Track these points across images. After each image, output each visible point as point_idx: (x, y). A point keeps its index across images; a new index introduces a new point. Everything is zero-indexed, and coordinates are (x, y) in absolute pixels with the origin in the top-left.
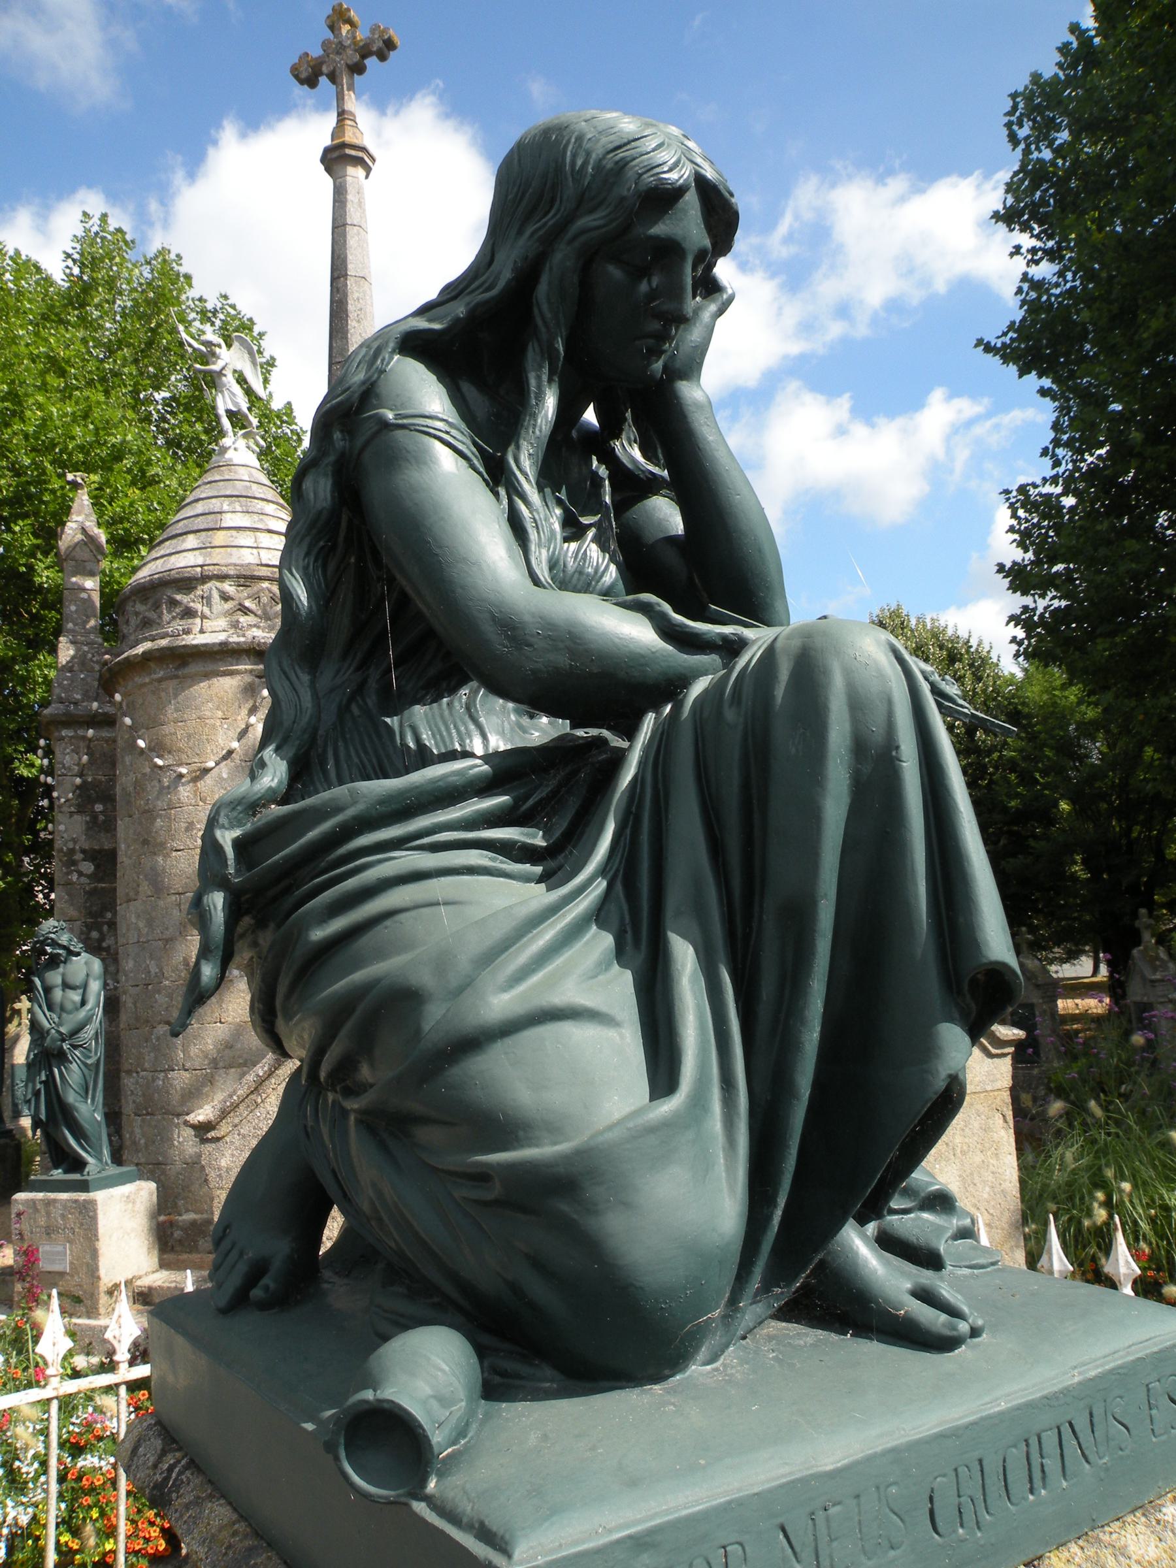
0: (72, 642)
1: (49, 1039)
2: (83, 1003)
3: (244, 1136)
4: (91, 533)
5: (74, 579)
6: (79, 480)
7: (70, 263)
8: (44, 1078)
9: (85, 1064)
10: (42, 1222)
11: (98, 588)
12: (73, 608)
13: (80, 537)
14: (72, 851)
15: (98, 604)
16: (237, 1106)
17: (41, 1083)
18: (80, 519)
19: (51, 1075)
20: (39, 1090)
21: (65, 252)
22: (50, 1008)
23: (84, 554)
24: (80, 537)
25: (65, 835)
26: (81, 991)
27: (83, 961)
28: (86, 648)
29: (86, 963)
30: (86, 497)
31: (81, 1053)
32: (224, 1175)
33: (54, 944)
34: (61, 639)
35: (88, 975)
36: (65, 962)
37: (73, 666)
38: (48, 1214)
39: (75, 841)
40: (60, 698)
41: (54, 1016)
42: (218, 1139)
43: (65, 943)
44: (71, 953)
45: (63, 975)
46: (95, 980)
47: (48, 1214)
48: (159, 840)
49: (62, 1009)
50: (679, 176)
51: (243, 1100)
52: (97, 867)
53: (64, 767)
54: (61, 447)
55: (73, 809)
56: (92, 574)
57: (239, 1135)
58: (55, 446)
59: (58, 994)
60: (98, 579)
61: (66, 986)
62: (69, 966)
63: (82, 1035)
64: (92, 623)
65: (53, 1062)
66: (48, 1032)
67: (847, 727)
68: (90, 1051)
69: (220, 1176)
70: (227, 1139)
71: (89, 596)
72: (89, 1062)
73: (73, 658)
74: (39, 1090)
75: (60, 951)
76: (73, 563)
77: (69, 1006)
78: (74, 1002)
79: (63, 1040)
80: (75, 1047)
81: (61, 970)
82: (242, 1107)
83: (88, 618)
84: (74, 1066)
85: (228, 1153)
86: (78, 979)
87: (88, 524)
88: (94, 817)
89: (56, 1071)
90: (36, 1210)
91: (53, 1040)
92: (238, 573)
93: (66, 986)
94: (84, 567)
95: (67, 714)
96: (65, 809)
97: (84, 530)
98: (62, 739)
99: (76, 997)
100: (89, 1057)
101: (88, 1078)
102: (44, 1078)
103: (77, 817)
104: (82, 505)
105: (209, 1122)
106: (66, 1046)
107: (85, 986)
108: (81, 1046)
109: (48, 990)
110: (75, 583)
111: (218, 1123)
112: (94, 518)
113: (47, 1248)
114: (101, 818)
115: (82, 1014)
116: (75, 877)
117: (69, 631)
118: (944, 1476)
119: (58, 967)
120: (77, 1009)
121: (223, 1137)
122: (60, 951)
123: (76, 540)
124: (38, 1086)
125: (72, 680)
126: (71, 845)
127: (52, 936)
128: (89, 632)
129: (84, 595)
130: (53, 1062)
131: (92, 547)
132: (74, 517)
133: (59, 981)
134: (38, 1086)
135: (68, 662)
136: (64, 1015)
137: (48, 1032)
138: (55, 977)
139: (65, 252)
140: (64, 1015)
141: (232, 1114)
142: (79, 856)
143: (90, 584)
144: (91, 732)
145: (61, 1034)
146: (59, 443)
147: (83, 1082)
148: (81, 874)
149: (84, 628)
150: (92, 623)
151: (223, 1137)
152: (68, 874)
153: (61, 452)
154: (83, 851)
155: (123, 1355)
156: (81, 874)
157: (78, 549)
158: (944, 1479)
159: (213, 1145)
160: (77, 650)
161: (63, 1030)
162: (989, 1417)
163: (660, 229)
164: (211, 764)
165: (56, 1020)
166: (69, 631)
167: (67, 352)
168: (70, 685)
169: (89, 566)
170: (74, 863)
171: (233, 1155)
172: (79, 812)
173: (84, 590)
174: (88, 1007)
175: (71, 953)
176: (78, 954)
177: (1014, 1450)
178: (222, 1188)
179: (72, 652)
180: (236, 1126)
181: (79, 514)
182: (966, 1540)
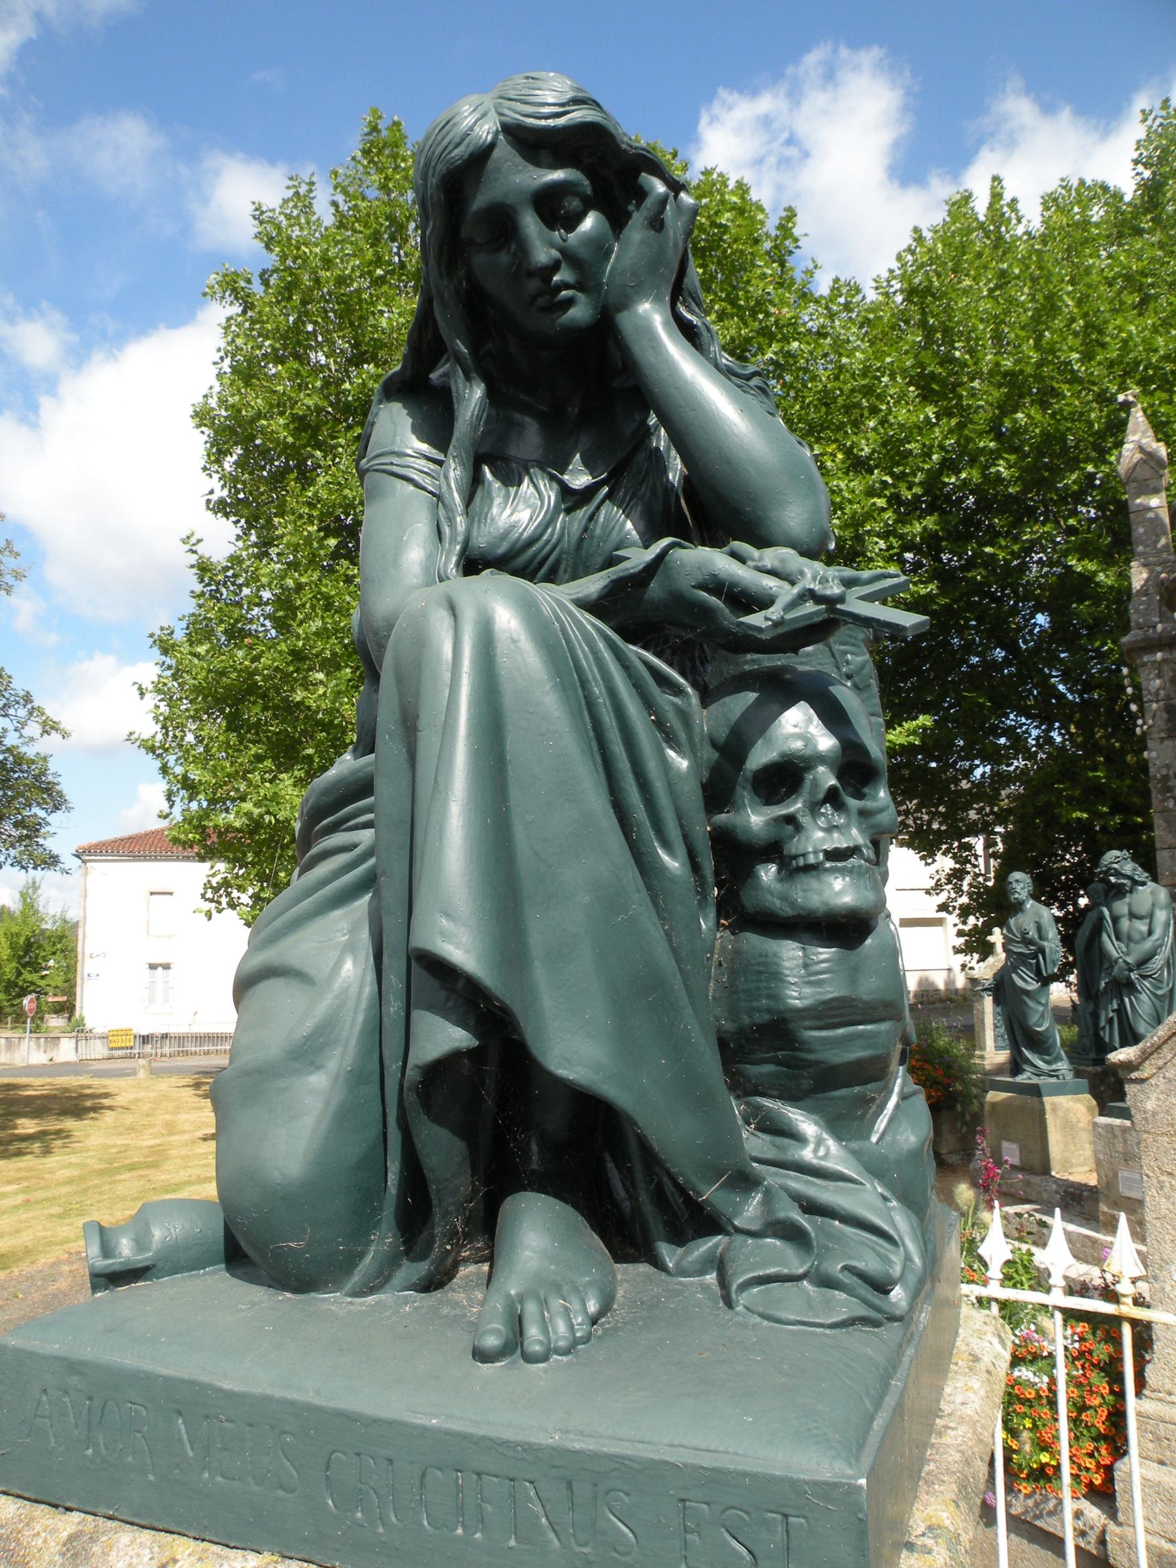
0: (1145, 565)
1: (1116, 969)
2: (1150, 933)
3: (1170, 1081)
4: (1149, 450)
5: (1138, 501)
6: (1131, 398)
7: (1140, 168)
8: (1115, 1007)
9: (1155, 995)
10: (1120, 1147)
11: (1165, 504)
12: (1141, 530)
13: (1138, 456)
15: (1167, 520)
16: (1159, 1047)
17: (1113, 1011)
18: (1136, 438)
19: (1122, 1004)
20: (1112, 1018)
21: (916, 230)
22: (1118, 938)
23: (1146, 472)
25: (1158, 762)
26: (1147, 921)
27: (1149, 890)
28: (1159, 569)
29: (1152, 893)
30: (1140, 413)
31: (1151, 983)
32: (1150, 1118)
33: (1118, 874)
34: (1132, 564)
35: (1153, 905)
36: (1131, 892)
37: (1147, 590)
38: (1125, 1140)
39: (1168, 766)
40: (1138, 623)
41: (1122, 945)
42: (1142, 1081)
43: (1129, 873)
44: (1136, 883)
45: (1129, 905)
46: (1161, 909)
47: (1125, 1140)
49: (1130, 938)
50: (486, 131)
51: (1165, 1042)
53: (1150, 693)
54: (1144, 363)
55: (1163, 735)
56: (1156, 491)
57: (1164, 1078)
58: (1138, 364)
59: (1125, 924)
60: (1164, 494)
61: (1133, 916)
62: (1134, 895)
63: (1150, 965)
64: (1163, 541)
65: (1124, 991)
66: (1116, 961)
67: (395, 700)
68: (1161, 982)
69: (1146, 1119)
70: (1152, 1081)
71: (1157, 515)
72: (1159, 992)
73: (1147, 581)
74: (1112, 1018)
75: (1125, 881)
76: (1135, 484)
77: (1136, 936)
78: (1140, 932)
79: (1131, 970)
80: (1144, 977)
81: (1127, 900)
82: (1166, 1048)
83: (1158, 537)
84: (1143, 997)
85: (1153, 1096)
86: (1144, 909)
87: (1144, 441)
89: (1127, 1000)
90: (1115, 1136)
91: (1121, 970)
93: (1133, 916)
94: (1148, 486)
95: (1146, 639)
96: (1155, 736)
97: (1141, 449)
98: (1144, 665)
99: (1143, 927)
100: (1160, 988)
101: (1160, 1010)
102: (1115, 1007)
103: (1168, 743)
104: (1137, 424)
105: (1130, 1062)
106: (1133, 976)
107: (1151, 916)
108: (1150, 976)
109: (1115, 920)
110: (1140, 505)
111: (1140, 1064)
112: (1150, 433)
113: (1126, 1174)
115: (1148, 945)
117: (1141, 554)
118: (345, 1453)
119: (1124, 896)
120: (1144, 939)
121: (1147, 1079)
122: (1125, 881)
123: (1135, 460)
124: (1111, 1014)
125: (1148, 603)
126: (1164, 772)
127: (1116, 866)
128: (1161, 551)
129: (1151, 515)
130: (1124, 991)
131: (1152, 464)
132: (1131, 438)
133: (1125, 910)
134: (1111, 1014)
135: (1142, 586)
136: (1132, 945)
137: (1116, 961)
138: (1121, 907)
139: (916, 230)
140: (1132, 945)
141: (1155, 1056)
143: (1154, 502)
144: (1159, 655)
145: (1127, 963)
146: (1141, 361)
147: (1154, 1013)
149: (1155, 547)
150: (1163, 541)
151: (1147, 1079)
152: (1164, 801)
153: (1146, 368)
155: (995, 1272)
157: (1138, 469)
158: (344, 1457)
159: (1138, 1087)
160: (1151, 572)
161: (1129, 960)
162: (405, 1425)
163: (480, 201)
165: (1124, 949)
166: (1141, 554)
167: (1140, 264)
168: (1146, 609)
169: (1152, 483)
171: (1158, 1099)
173: (1150, 509)
174: (1155, 936)
175: (1136, 883)
176: (1143, 884)
177: (438, 1473)
178: (1148, 1132)
179: (1145, 575)
180: (1160, 1068)
181: (1135, 432)
182: (363, 1526)
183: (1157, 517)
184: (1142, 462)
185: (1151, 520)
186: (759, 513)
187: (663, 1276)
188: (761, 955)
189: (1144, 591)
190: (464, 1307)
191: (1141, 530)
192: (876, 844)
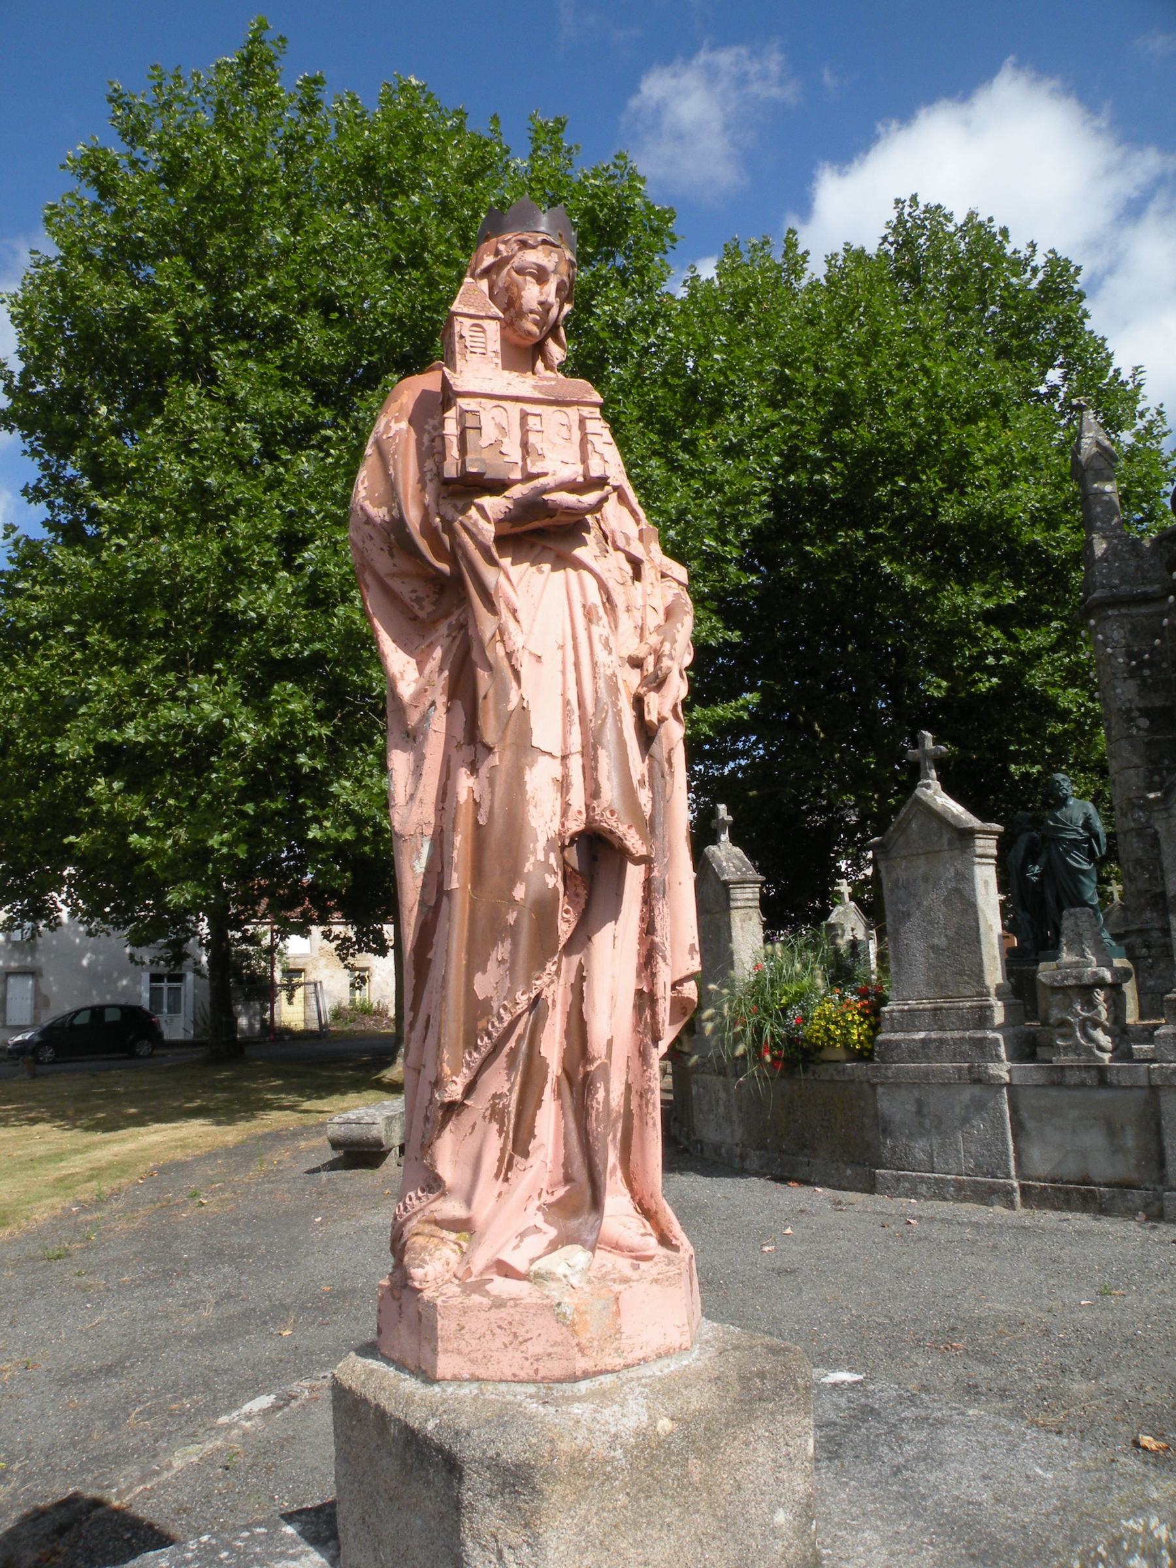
0: (1104, 537)
12: (1099, 509)
13: (1095, 449)
14: (1129, 710)
23: (1100, 464)
24: (1095, 449)
39: (1130, 701)
43: (588, 430)
48: (1076, 287)
52: (1152, 722)
56: (1109, 479)
73: (1106, 550)
88: (1144, 680)
92: (1071, 1168)
97: (1098, 444)
103: (1129, 682)
114: (1150, 681)
116: (1134, 731)
129: (1106, 498)
142: (1136, 714)
143: (1108, 488)
148: (1139, 729)
154: (1139, 709)
156: (1139, 729)
160: (1109, 543)
164: (457, 1096)
170: (1132, 720)
172: (1131, 677)
173: (1105, 493)
183: (1111, 501)
184: (1098, 455)
185: (1107, 502)
186: (538, 549)
187: (287, 1506)
188: (568, 1179)
189: (1104, 558)
190: (602, 341)
191: (1099, 509)
192: (977, 1081)
